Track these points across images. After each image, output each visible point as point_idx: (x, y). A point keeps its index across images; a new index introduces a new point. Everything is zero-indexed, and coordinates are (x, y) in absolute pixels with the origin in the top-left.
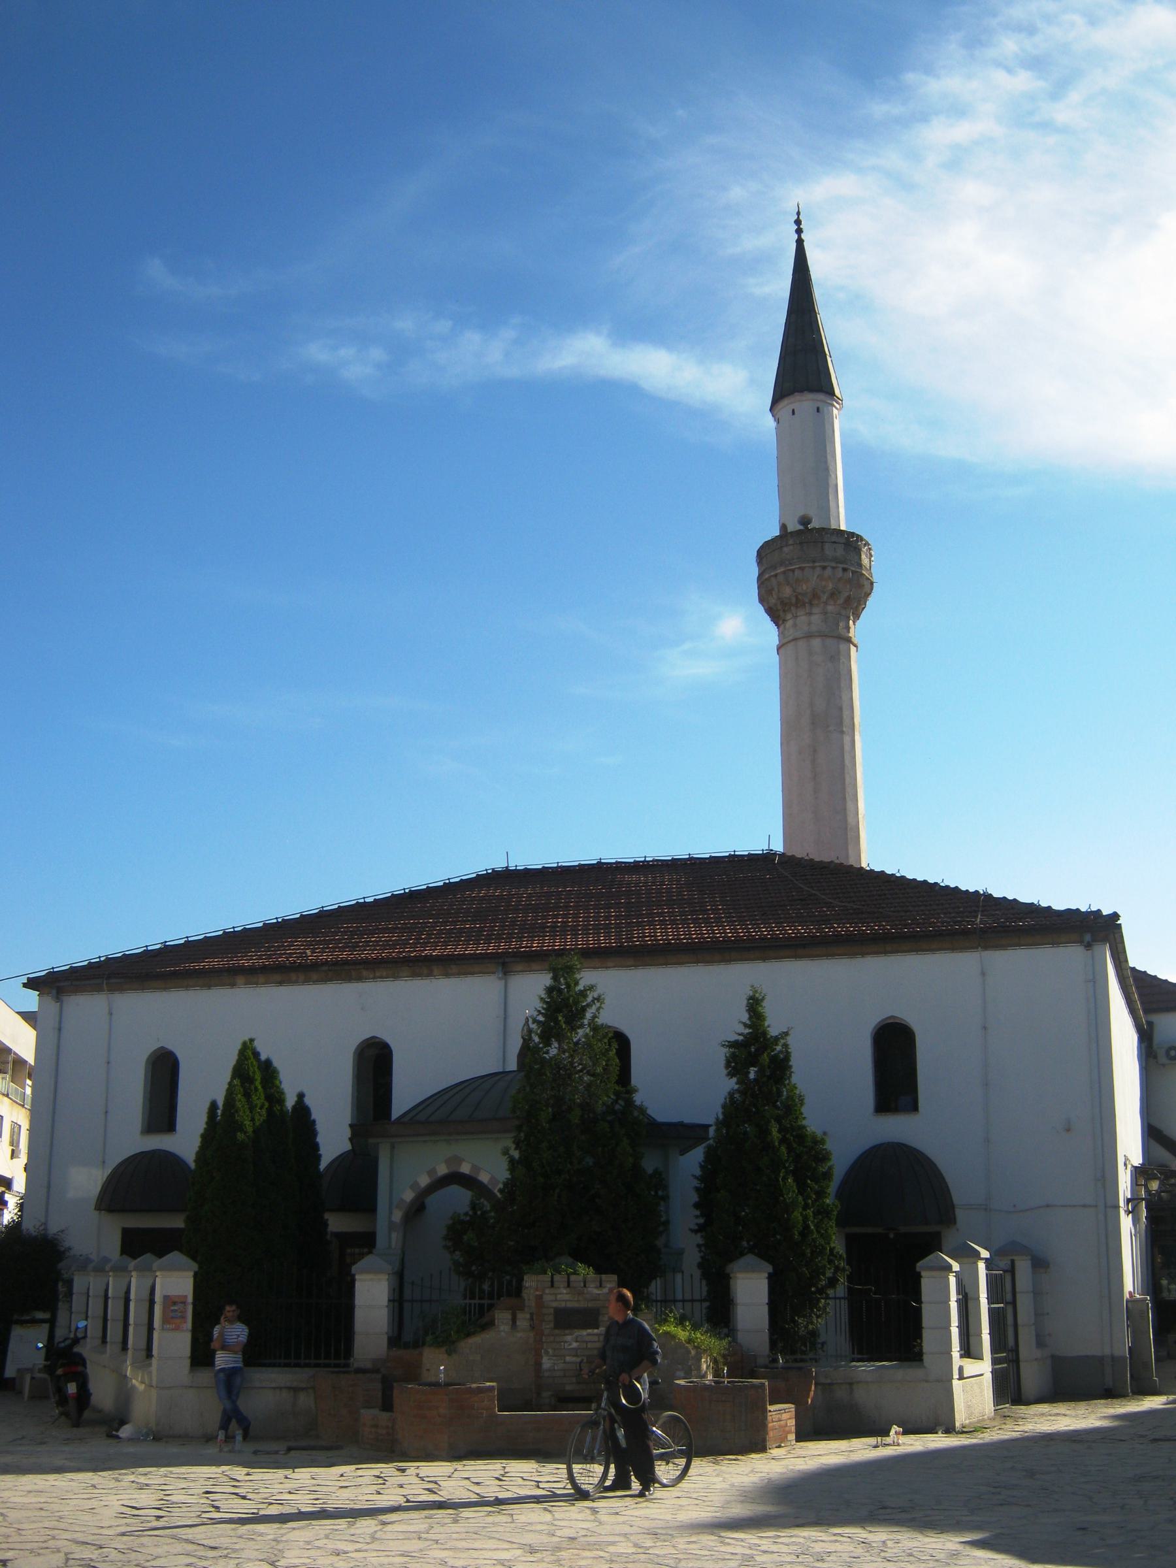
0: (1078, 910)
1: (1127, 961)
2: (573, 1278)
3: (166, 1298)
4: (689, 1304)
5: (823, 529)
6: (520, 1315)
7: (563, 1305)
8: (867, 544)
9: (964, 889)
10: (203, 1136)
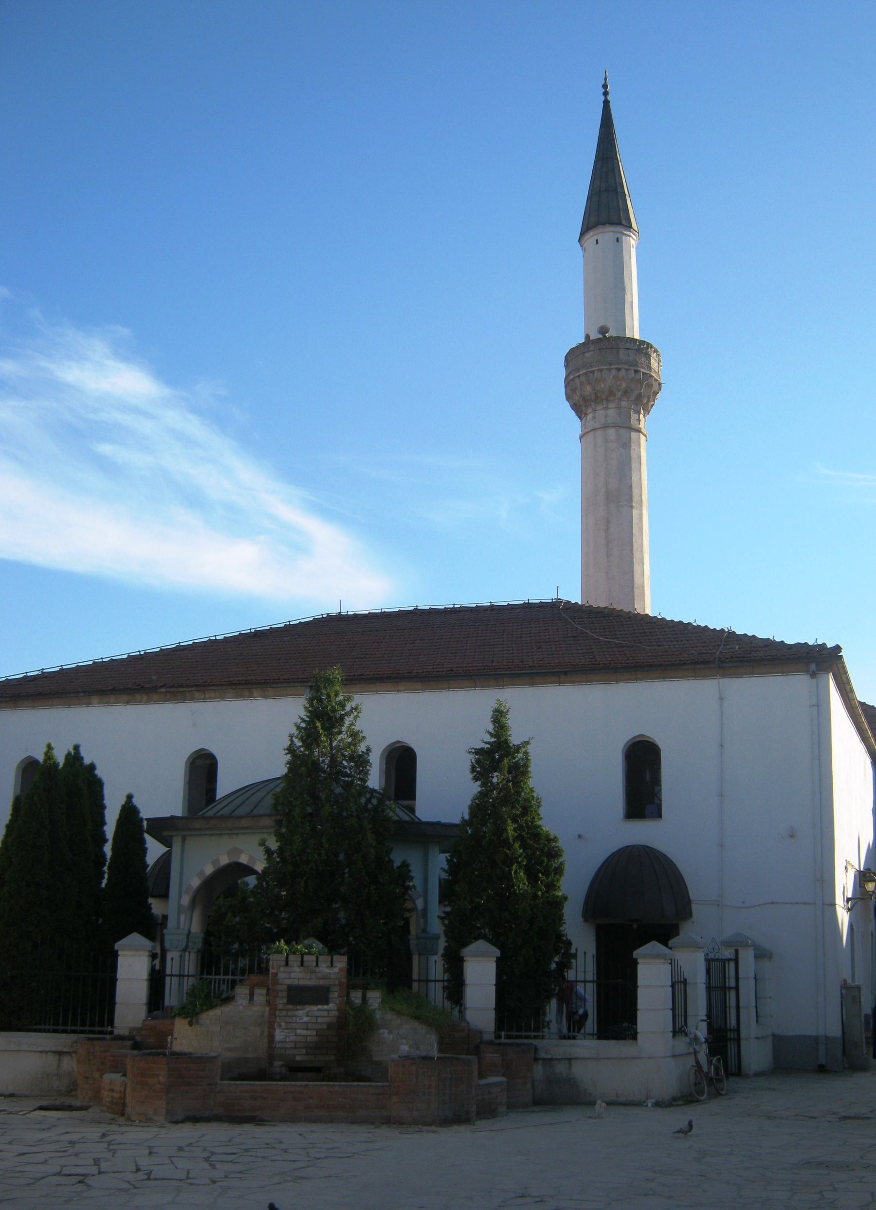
2: (306, 958)
4: (578, 979)
6: (257, 991)
7: (296, 982)
8: (656, 351)
10: (8, 826)
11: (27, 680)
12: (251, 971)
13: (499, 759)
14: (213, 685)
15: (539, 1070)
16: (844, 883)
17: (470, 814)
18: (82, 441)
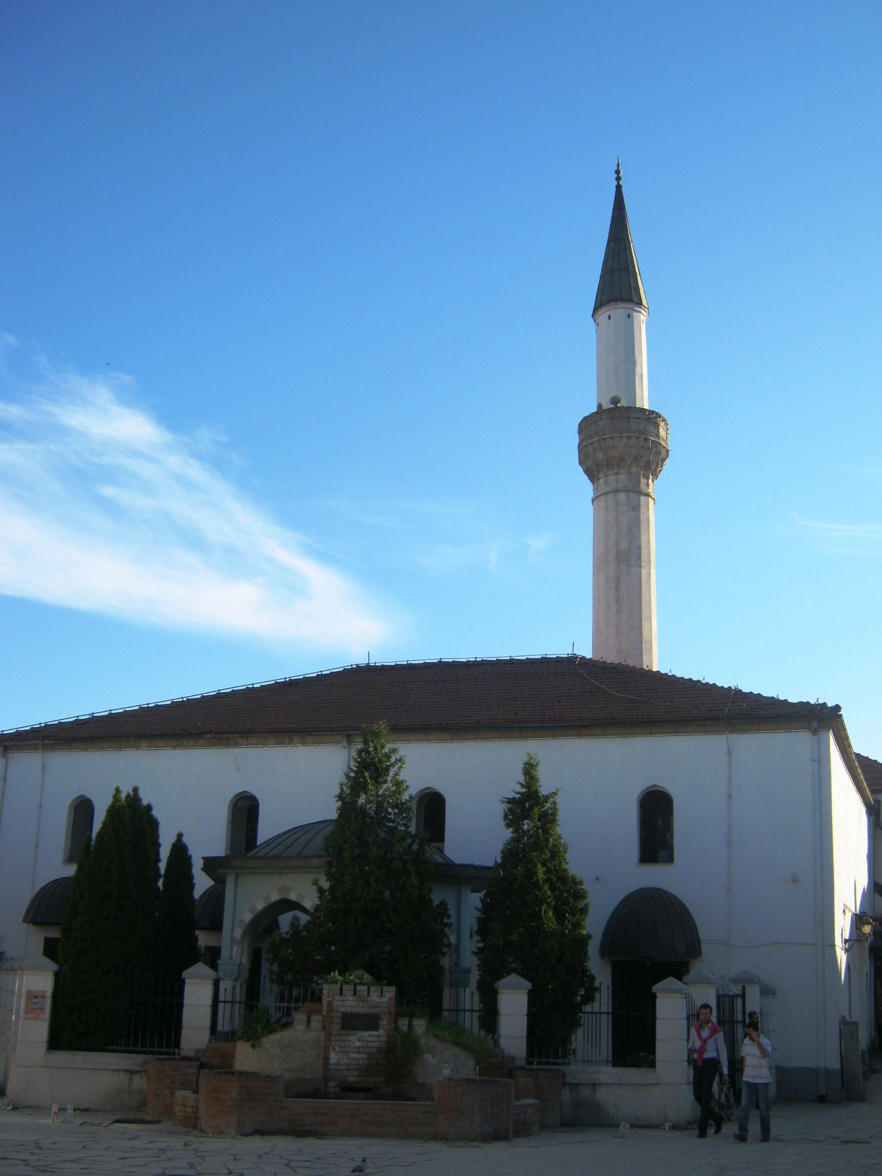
0: (808, 703)
1: (850, 746)
2: (359, 988)
3: (28, 991)
5: (630, 407)
6: (314, 1018)
7: (349, 1010)
9: (720, 685)
11: (79, 724)
12: (304, 1000)
13: (529, 808)
14: (256, 732)
15: (566, 1094)
16: (842, 926)
17: (502, 858)
18: (87, 484)
